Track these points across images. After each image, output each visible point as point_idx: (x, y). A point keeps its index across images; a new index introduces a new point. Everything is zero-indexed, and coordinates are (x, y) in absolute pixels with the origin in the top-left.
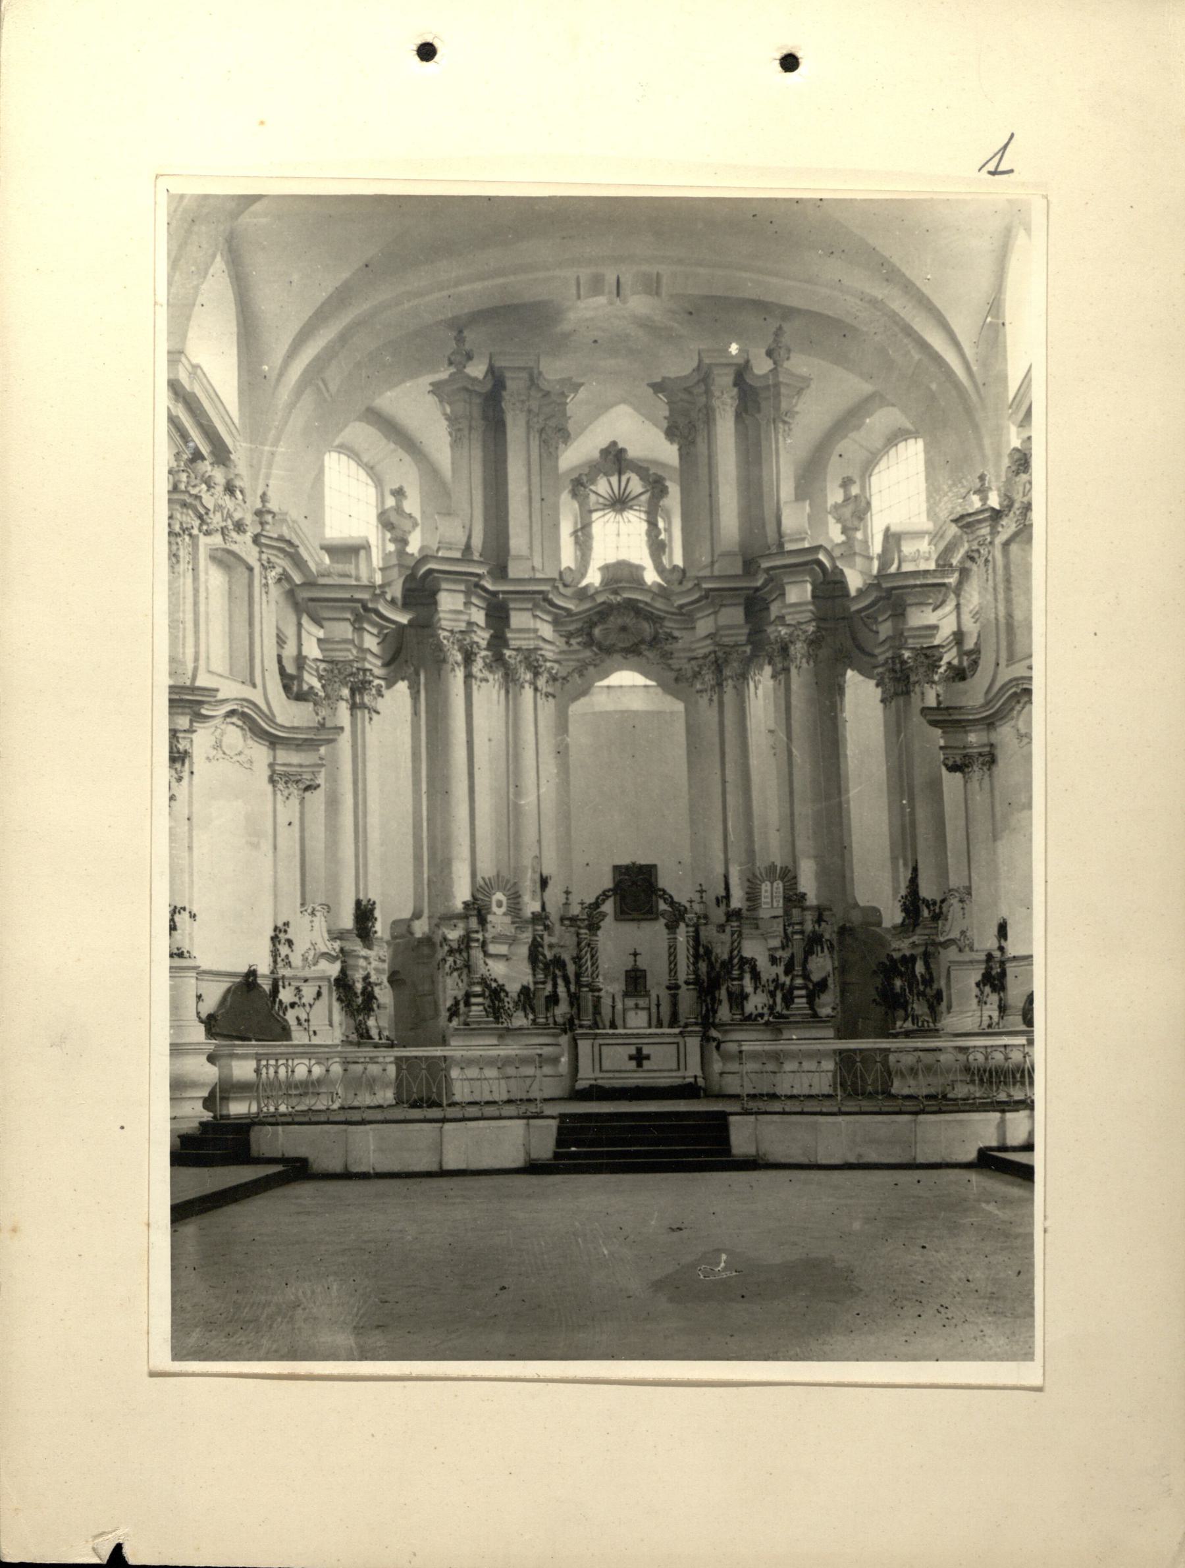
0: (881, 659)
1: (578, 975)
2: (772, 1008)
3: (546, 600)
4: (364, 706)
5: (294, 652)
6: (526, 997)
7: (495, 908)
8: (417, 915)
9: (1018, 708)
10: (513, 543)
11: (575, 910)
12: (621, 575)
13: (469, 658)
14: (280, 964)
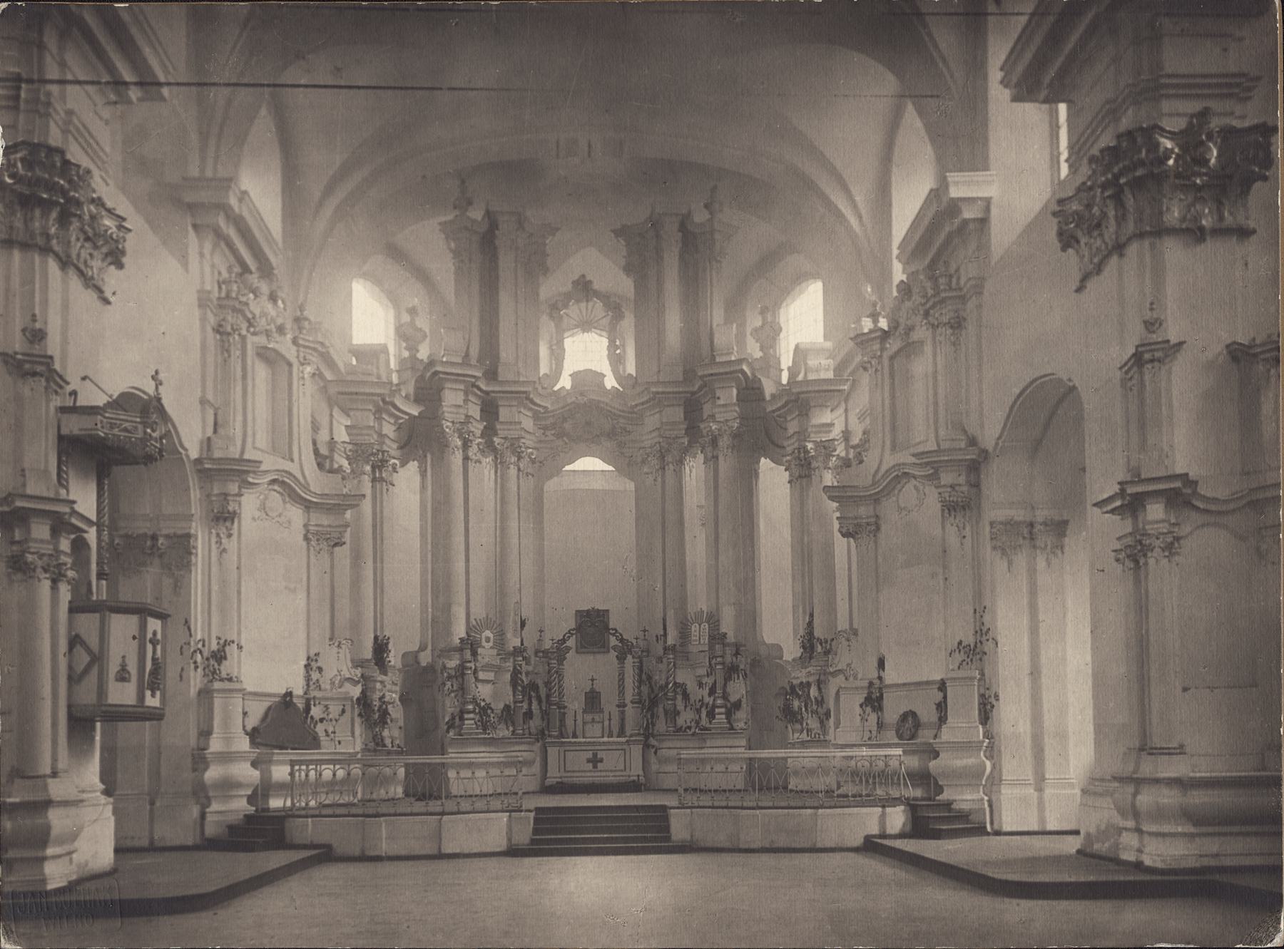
0: (789, 450)
1: (548, 696)
2: (697, 723)
3: (527, 398)
4: (382, 480)
5: (327, 438)
6: (508, 714)
7: (484, 643)
8: (423, 648)
9: (899, 486)
10: (503, 355)
11: (547, 645)
12: (587, 379)
13: (466, 445)
14: (312, 687)
